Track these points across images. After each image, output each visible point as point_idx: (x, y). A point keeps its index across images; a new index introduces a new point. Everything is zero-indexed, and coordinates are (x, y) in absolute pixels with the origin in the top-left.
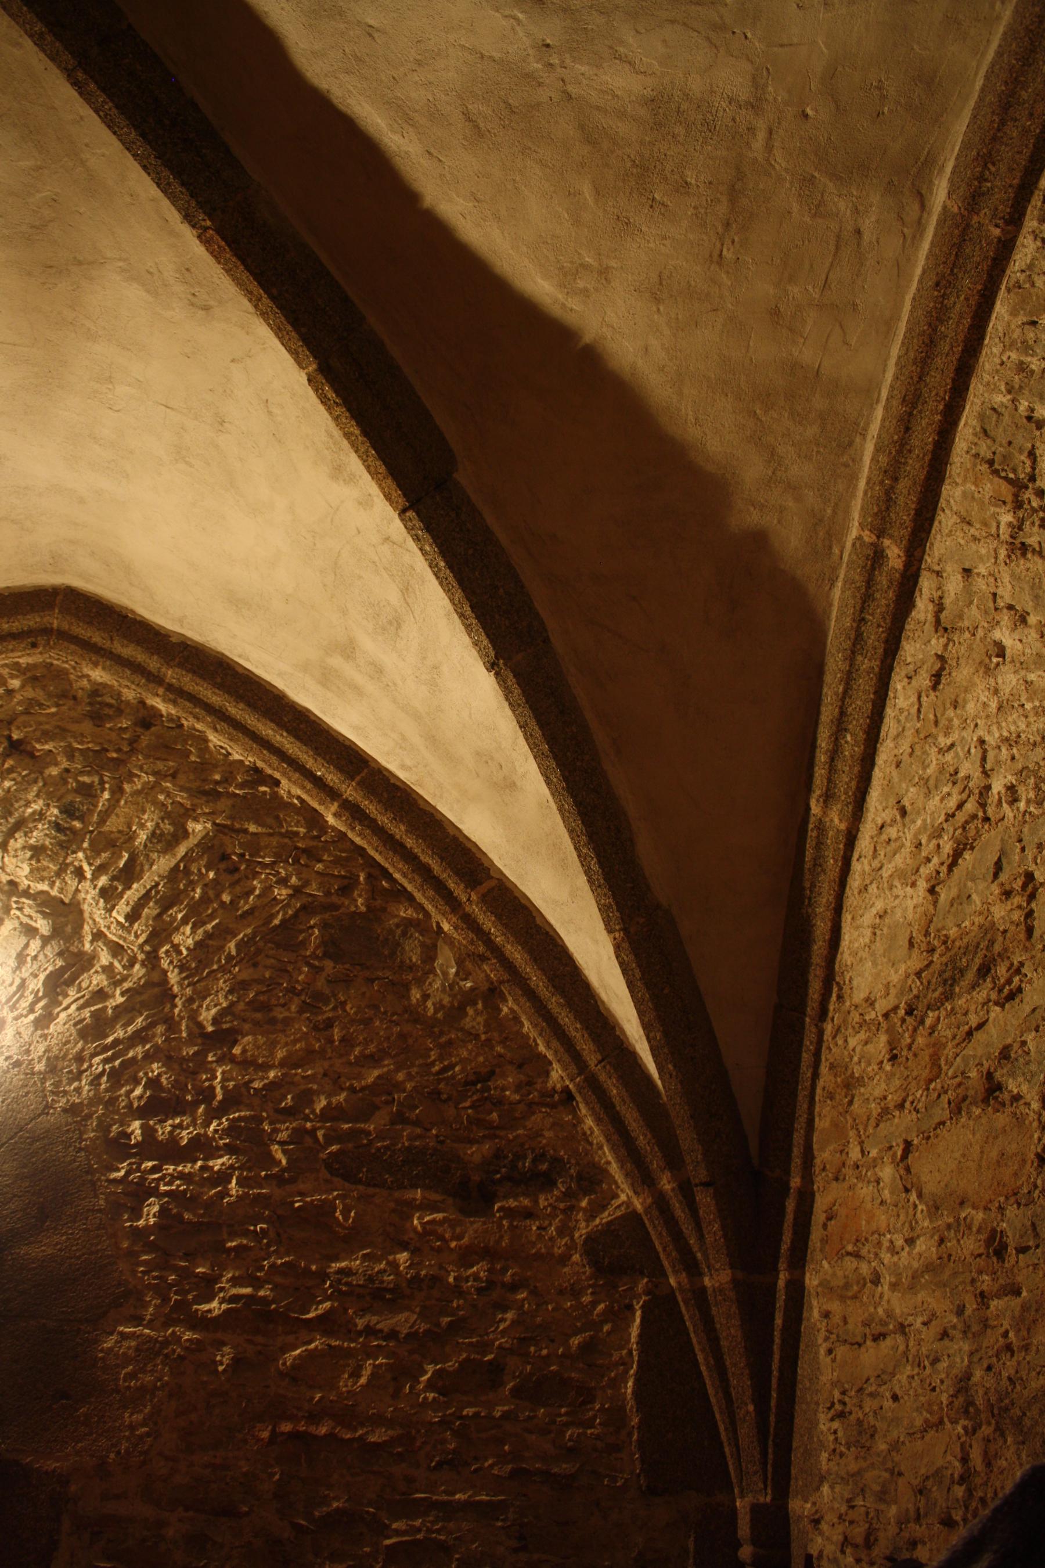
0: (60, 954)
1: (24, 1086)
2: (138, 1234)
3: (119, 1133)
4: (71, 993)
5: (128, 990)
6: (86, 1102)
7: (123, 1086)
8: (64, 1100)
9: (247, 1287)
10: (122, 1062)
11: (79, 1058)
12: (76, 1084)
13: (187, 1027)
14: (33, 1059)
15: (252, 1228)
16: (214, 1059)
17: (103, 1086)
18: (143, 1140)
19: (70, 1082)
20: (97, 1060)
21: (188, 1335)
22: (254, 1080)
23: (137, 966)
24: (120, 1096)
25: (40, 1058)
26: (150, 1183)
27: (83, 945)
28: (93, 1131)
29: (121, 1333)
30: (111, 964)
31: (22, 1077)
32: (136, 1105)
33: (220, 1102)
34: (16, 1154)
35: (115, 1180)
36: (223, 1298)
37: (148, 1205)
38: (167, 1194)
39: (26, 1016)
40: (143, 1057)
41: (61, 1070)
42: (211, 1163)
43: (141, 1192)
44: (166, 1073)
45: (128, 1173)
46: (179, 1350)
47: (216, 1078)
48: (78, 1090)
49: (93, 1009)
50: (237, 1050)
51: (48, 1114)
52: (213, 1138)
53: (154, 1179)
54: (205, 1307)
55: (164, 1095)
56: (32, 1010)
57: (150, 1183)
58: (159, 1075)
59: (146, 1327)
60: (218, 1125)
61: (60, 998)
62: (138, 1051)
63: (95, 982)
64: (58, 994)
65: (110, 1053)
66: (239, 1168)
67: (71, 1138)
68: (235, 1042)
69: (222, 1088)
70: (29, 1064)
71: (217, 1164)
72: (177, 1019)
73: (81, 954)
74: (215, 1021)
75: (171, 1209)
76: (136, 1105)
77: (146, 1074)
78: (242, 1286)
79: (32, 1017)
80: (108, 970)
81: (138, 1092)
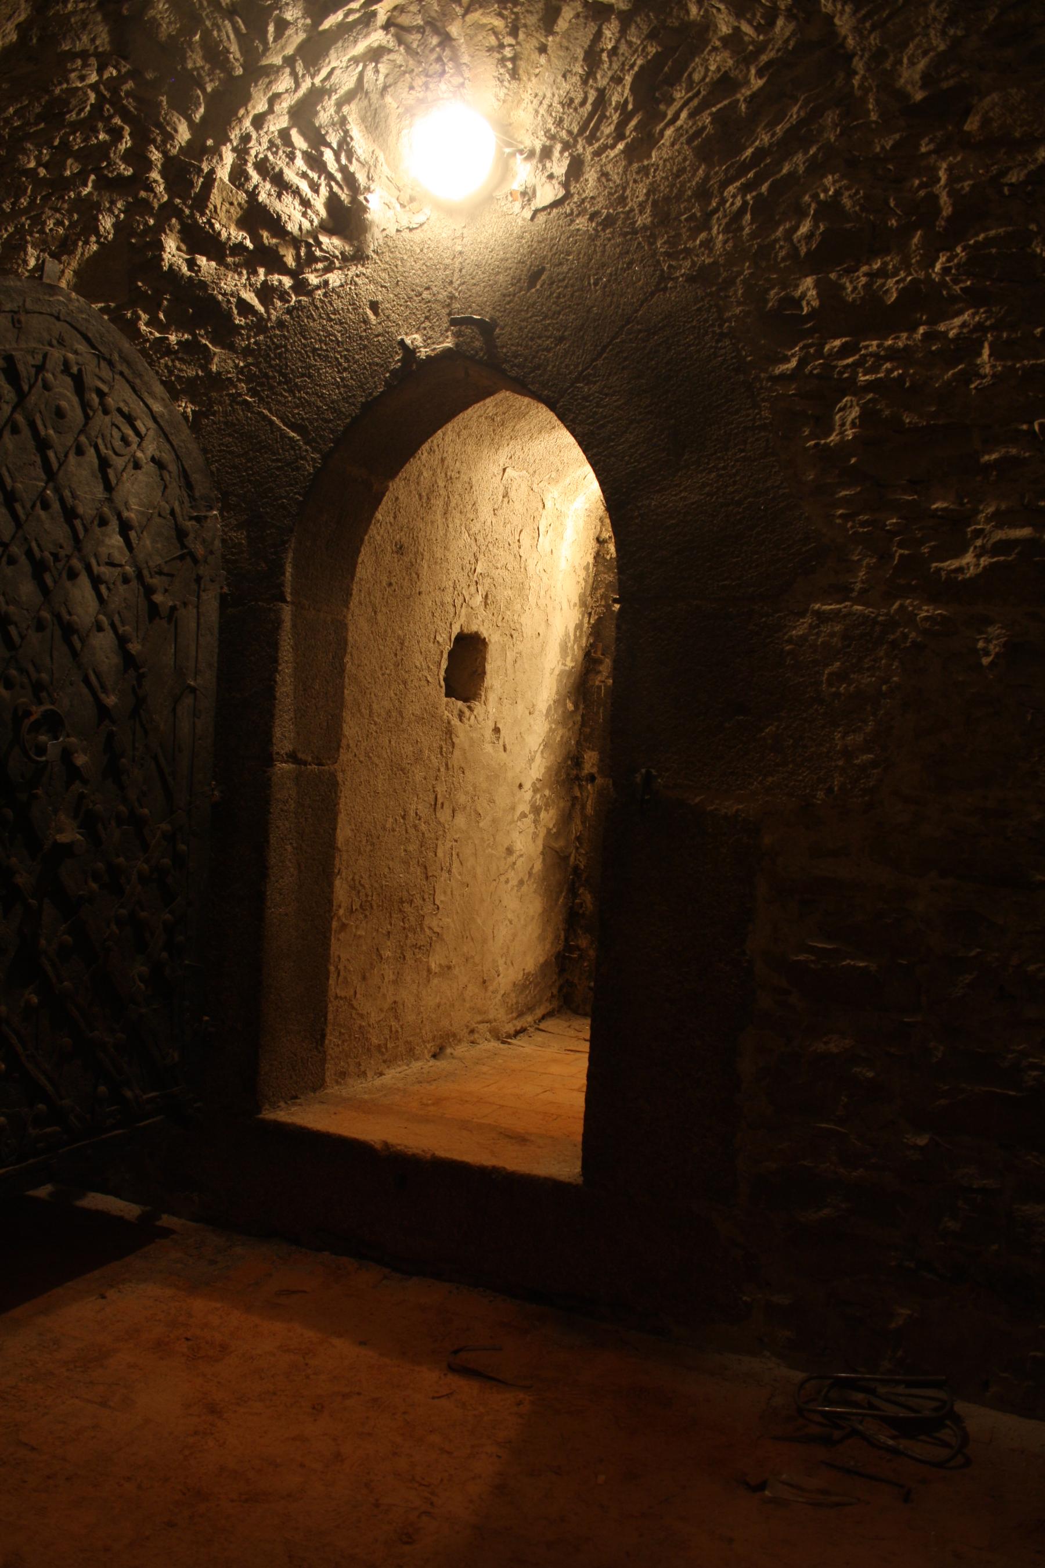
0: (652, 36)
1: (622, 255)
2: (828, 456)
3: (781, 301)
4: (677, 95)
5: (769, 64)
6: (721, 261)
7: (778, 224)
8: (688, 263)
9: (1023, 527)
10: (771, 186)
11: (703, 194)
12: (703, 235)
13: (877, 101)
14: (632, 210)
15: (1025, 427)
16: (931, 147)
17: (747, 231)
18: (820, 305)
19: (697, 230)
20: (731, 189)
21: (926, 611)
22: (1009, 169)
23: (780, 22)
24: (776, 241)
25: (642, 206)
26: (841, 373)
27: (688, 12)
28: (739, 303)
29: (818, 614)
30: (737, 30)
31: (619, 240)
32: (803, 250)
33: (949, 219)
34: (626, 359)
35: (782, 376)
36: (983, 547)
37: (841, 410)
38: (869, 386)
39: (613, 147)
40: (807, 170)
41: (677, 218)
42: (942, 327)
43: (824, 391)
44: (848, 188)
45: (802, 363)
46: (913, 635)
47: (939, 179)
48: (708, 244)
49: (714, 109)
50: (972, 125)
51: (665, 289)
52: (943, 284)
53: (848, 366)
54: (953, 564)
55: (849, 226)
56: (620, 135)
57: (841, 373)
58: (838, 193)
59: (856, 601)
60: (949, 260)
61: (662, 107)
62: (799, 161)
63: (713, 68)
64: (658, 102)
65: (750, 175)
66: (992, 328)
67: (706, 321)
68: (967, 112)
69: (949, 195)
70: (627, 218)
71: (952, 327)
72: (858, 93)
73: (686, 26)
74: (927, 80)
75: (881, 410)
76: (803, 250)
77: (815, 196)
78: (1013, 525)
79: (620, 146)
80: (733, 42)
81: (804, 229)
